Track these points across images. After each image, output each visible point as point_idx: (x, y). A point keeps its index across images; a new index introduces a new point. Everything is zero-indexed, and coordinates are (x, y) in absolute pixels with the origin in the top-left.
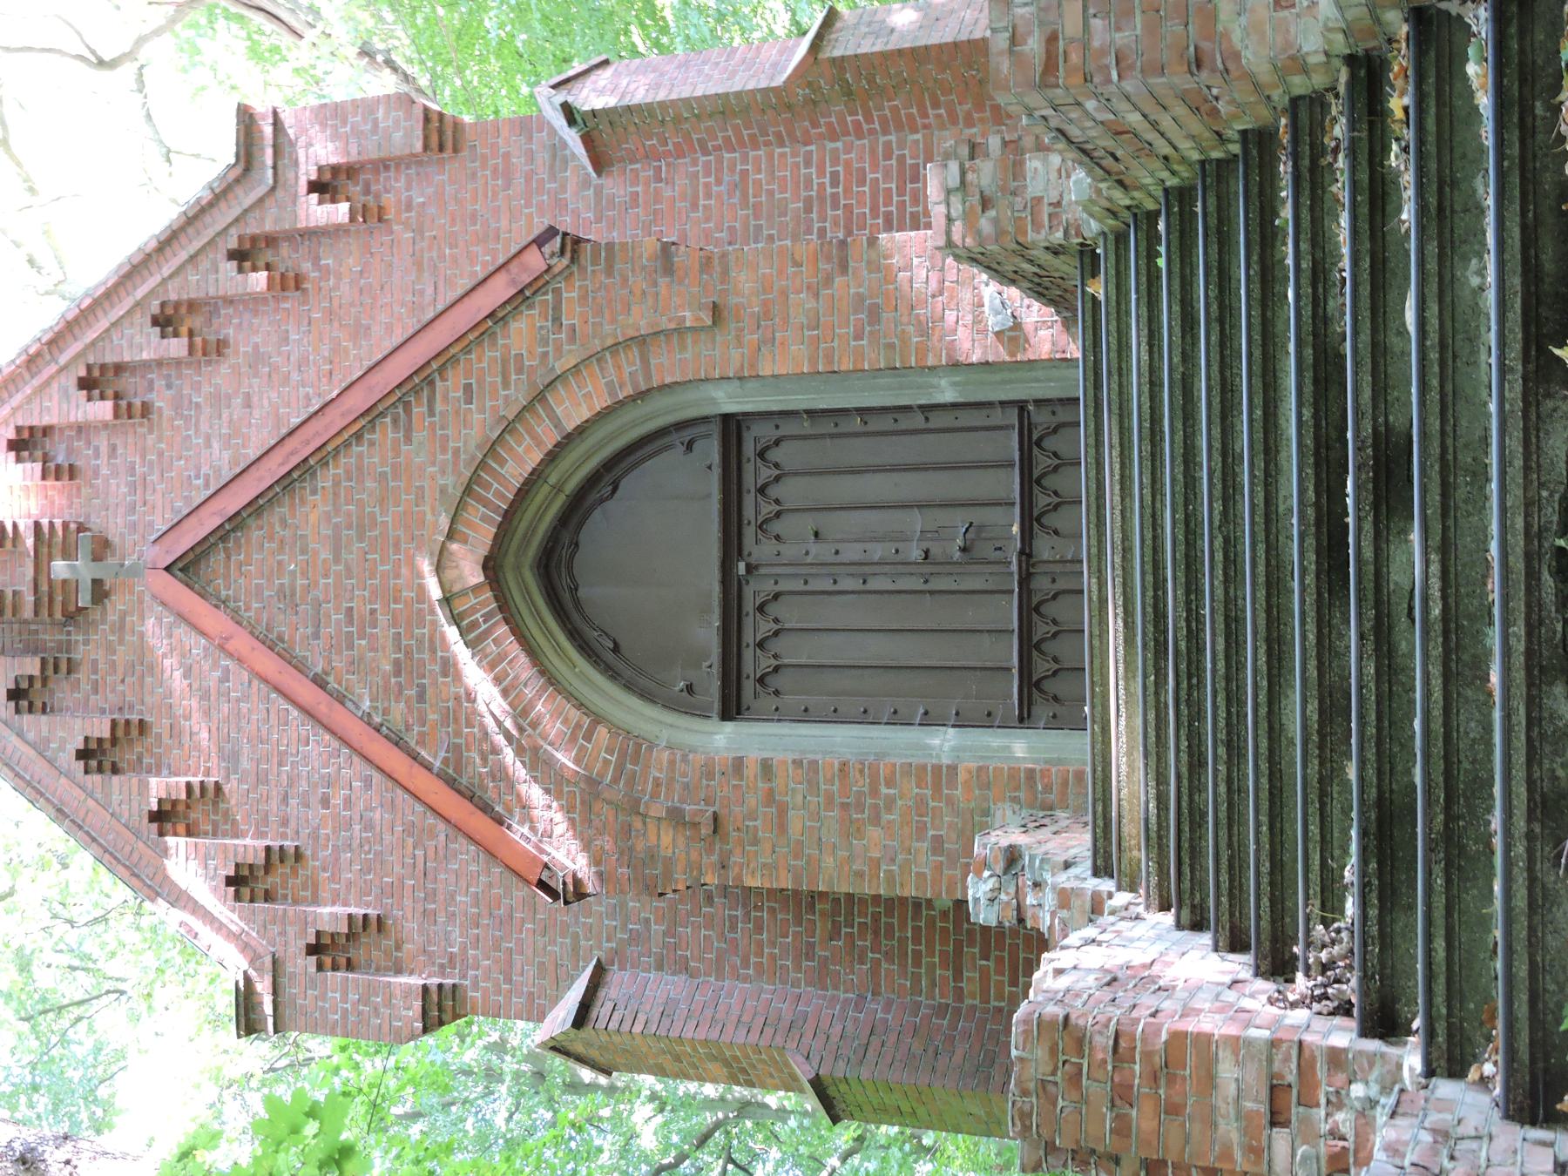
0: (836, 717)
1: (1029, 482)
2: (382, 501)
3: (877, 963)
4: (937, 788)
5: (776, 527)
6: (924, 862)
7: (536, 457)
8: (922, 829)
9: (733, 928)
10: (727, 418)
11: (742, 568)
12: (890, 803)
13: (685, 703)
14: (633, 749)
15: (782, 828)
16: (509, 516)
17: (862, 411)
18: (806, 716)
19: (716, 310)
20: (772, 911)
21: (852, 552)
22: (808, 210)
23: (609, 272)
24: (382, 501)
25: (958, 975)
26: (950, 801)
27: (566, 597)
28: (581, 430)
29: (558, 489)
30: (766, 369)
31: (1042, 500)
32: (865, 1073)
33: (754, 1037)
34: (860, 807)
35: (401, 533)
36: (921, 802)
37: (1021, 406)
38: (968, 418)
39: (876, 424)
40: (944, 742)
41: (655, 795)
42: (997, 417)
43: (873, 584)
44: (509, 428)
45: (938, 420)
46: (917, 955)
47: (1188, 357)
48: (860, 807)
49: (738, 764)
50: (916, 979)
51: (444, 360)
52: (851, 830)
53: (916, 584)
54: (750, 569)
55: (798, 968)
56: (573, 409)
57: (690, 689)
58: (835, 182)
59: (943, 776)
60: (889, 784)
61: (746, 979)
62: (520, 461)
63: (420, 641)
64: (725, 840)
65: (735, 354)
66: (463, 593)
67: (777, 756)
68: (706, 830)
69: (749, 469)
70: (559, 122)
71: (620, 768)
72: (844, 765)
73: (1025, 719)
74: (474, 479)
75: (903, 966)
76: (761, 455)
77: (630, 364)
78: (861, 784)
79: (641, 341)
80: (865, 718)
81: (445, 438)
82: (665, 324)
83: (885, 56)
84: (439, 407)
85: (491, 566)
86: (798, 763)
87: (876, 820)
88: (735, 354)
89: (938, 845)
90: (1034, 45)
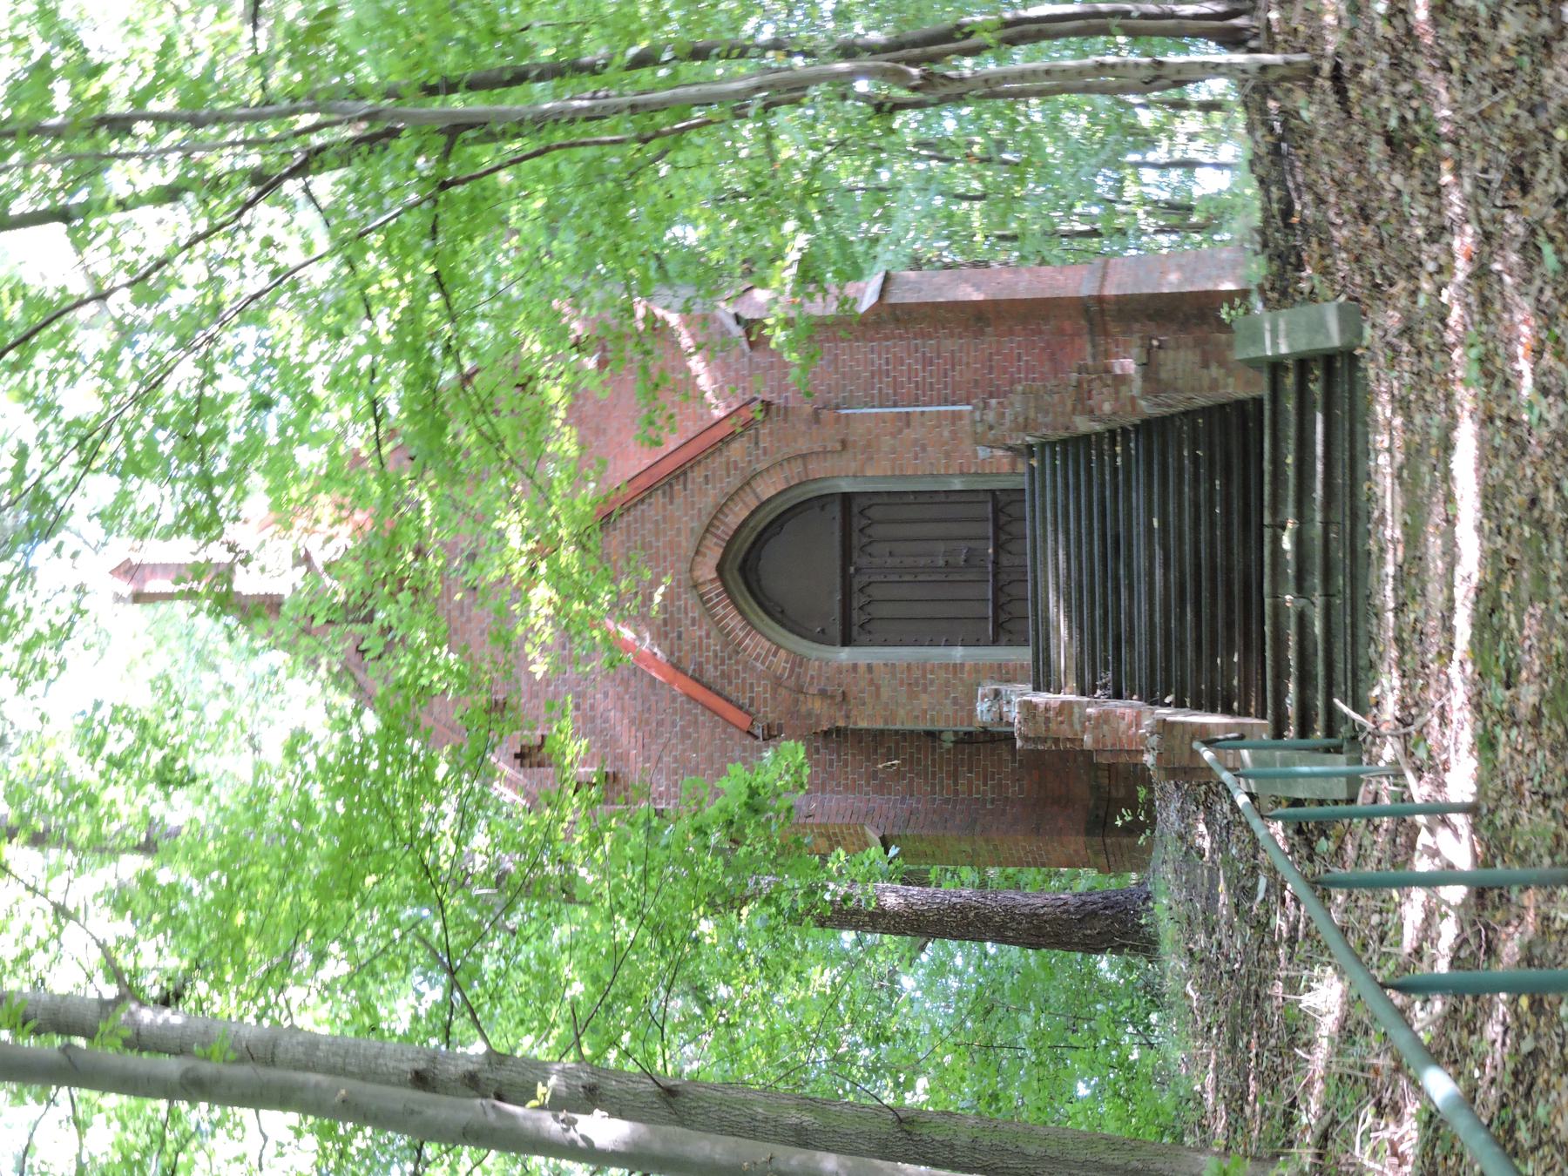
0: (901, 643)
1: (997, 528)
2: (657, 535)
3: (911, 779)
4: (955, 673)
5: (869, 549)
6: (949, 709)
7: (746, 513)
8: (948, 693)
9: (831, 765)
10: (845, 495)
11: (852, 569)
12: (932, 682)
13: (822, 638)
14: (799, 662)
15: (878, 695)
16: (730, 543)
17: (914, 492)
18: (885, 644)
19: (844, 443)
20: (854, 755)
21: (909, 561)
22: (873, 377)
23: (785, 420)
24: (657, 535)
25: (956, 783)
26: (961, 680)
27: (754, 585)
28: (769, 500)
29: (754, 529)
30: (869, 473)
31: (1003, 537)
32: (909, 832)
33: (847, 820)
34: (917, 684)
35: (668, 552)
36: (947, 681)
37: (993, 492)
38: (965, 498)
39: (921, 499)
40: (958, 653)
41: (811, 684)
42: (981, 497)
43: (920, 578)
44: (731, 498)
45: (953, 498)
46: (934, 774)
47: (1067, 498)
48: (917, 684)
49: (855, 667)
50: (933, 786)
51: (694, 462)
52: (912, 696)
53: (943, 578)
54: (857, 570)
55: (868, 784)
56: (767, 488)
57: (823, 631)
58: (887, 364)
59: (957, 668)
60: (932, 672)
61: (839, 793)
62: (736, 515)
63: (679, 608)
64: (848, 703)
65: (853, 465)
66: (704, 583)
67: (874, 662)
68: (839, 699)
69: (855, 520)
70: (731, 324)
71: (792, 670)
72: (909, 666)
73: (995, 642)
74: (711, 524)
75: (926, 779)
76: (861, 512)
77: (797, 467)
78: (917, 673)
79: (804, 457)
80: (917, 643)
81: (693, 503)
82: (817, 448)
83: (919, 305)
84: (689, 486)
85: (720, 568)
86: (886, 665)
87: (925, 690)
88: (853, 465)
89: (955, 701)
90: (1021, 420)
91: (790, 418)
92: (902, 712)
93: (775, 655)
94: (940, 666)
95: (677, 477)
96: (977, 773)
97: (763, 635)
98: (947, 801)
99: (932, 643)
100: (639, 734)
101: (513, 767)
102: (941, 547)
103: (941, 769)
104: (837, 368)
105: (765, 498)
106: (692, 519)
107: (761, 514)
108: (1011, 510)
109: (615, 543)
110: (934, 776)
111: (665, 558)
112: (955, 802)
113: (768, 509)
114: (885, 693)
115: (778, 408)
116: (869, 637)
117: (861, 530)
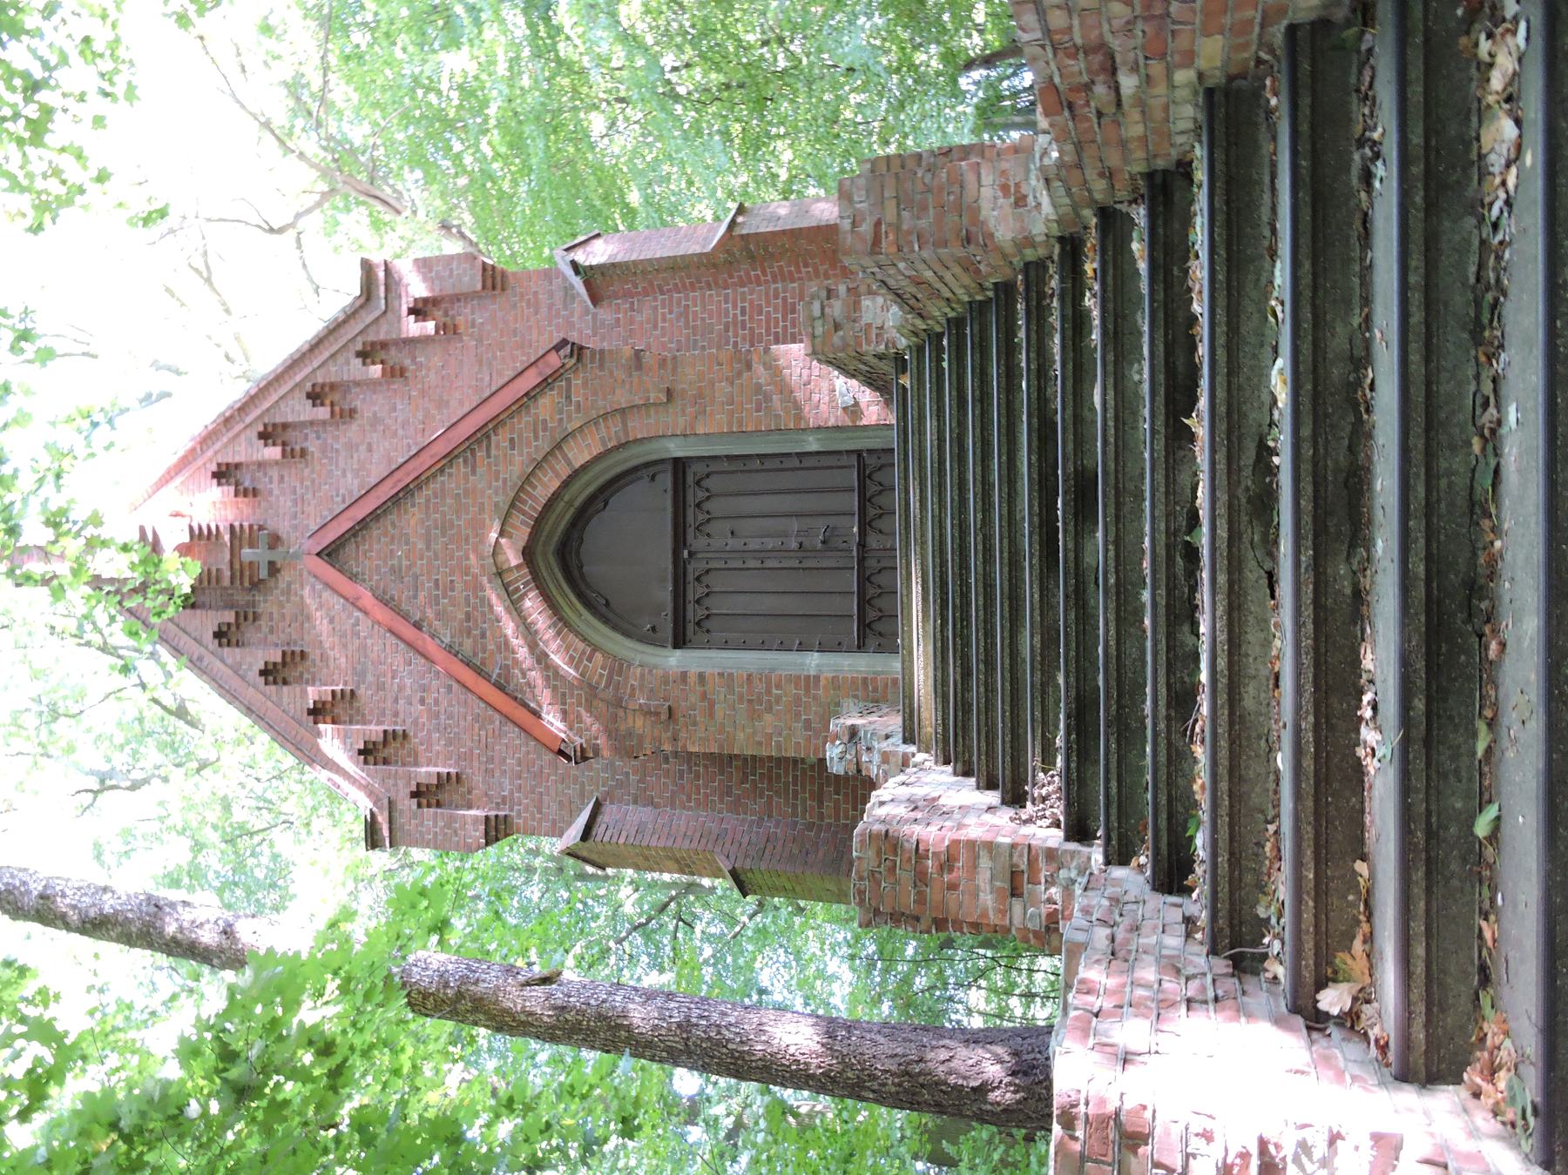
0: (745, 646)
1: (864, 500)
3: (770, 797)
4: (807, 688)
7: (556, 484)
8: (798, 715)
9: (682, 778)
10: (676, 460)
12: (778, 699)
13: (651, 638)
15: (711, 715)
16: (539, 522)
18: (726, 646)
19: (669, 393)
21: (754, 544)
22: (727, 330)
23: (601, 367)
26: (815, 698)
27: (576, 573)
28: (584, 467)
29: (570, 504)
30: (700, 430)
31: (872, 512)
36: (798, 699)
37: (859, 453)
39: (769, 464)
40: (813, 662)
42: (844, 460)
44: (538, 466)
45: (808, 462)
46: (796, 793)
47: (961, 424)
49: (684, 676)
50: (795, 807)
51: (497, 422)
52: (754, 716)
53: (795, 564)
55: (721, 801)
56: (579, 454)
57: (653, 629)
58: (743, 313)
59: (811, 682)
60: (778, 687)
61: (690, 809)
62: (545, 486)
65: (681, 420)
67: (708, 671)
68: (664, 717)
70: (569, 272)
72: (749, 676)
73: (861, 647)
74: (516, 498)
75: (787, 799)
76: (698, 483)
78: (760, 687)
79: (622, 412)
80: (763, 646)
81: (497, 472)
84: (493, 452)
86: (721, 675)
87: (769, 709)
91: (607, 365)
92: (741, 736)
93: (589, 660)
94: (789, 678)
95: (479, 441)
96: (846, 795)
97: (577, 634)
98: (810, 826)
99: (783, 647)
100: (483, 733)
101: (357, 764)
102: (795, 525)
103: (803, 787)
104: (687, 322)
105: (577, 465)
106: (496, 493)
107: (575, 487)
108: (878, 476)
109: (412, 522)
110: (795, 797)
111: (467, 540)
112: (820, 828)
113: (585, 478)
114: (719, 710)
115: (593, 352)
116: (706, 637)
117: (698, 505)
